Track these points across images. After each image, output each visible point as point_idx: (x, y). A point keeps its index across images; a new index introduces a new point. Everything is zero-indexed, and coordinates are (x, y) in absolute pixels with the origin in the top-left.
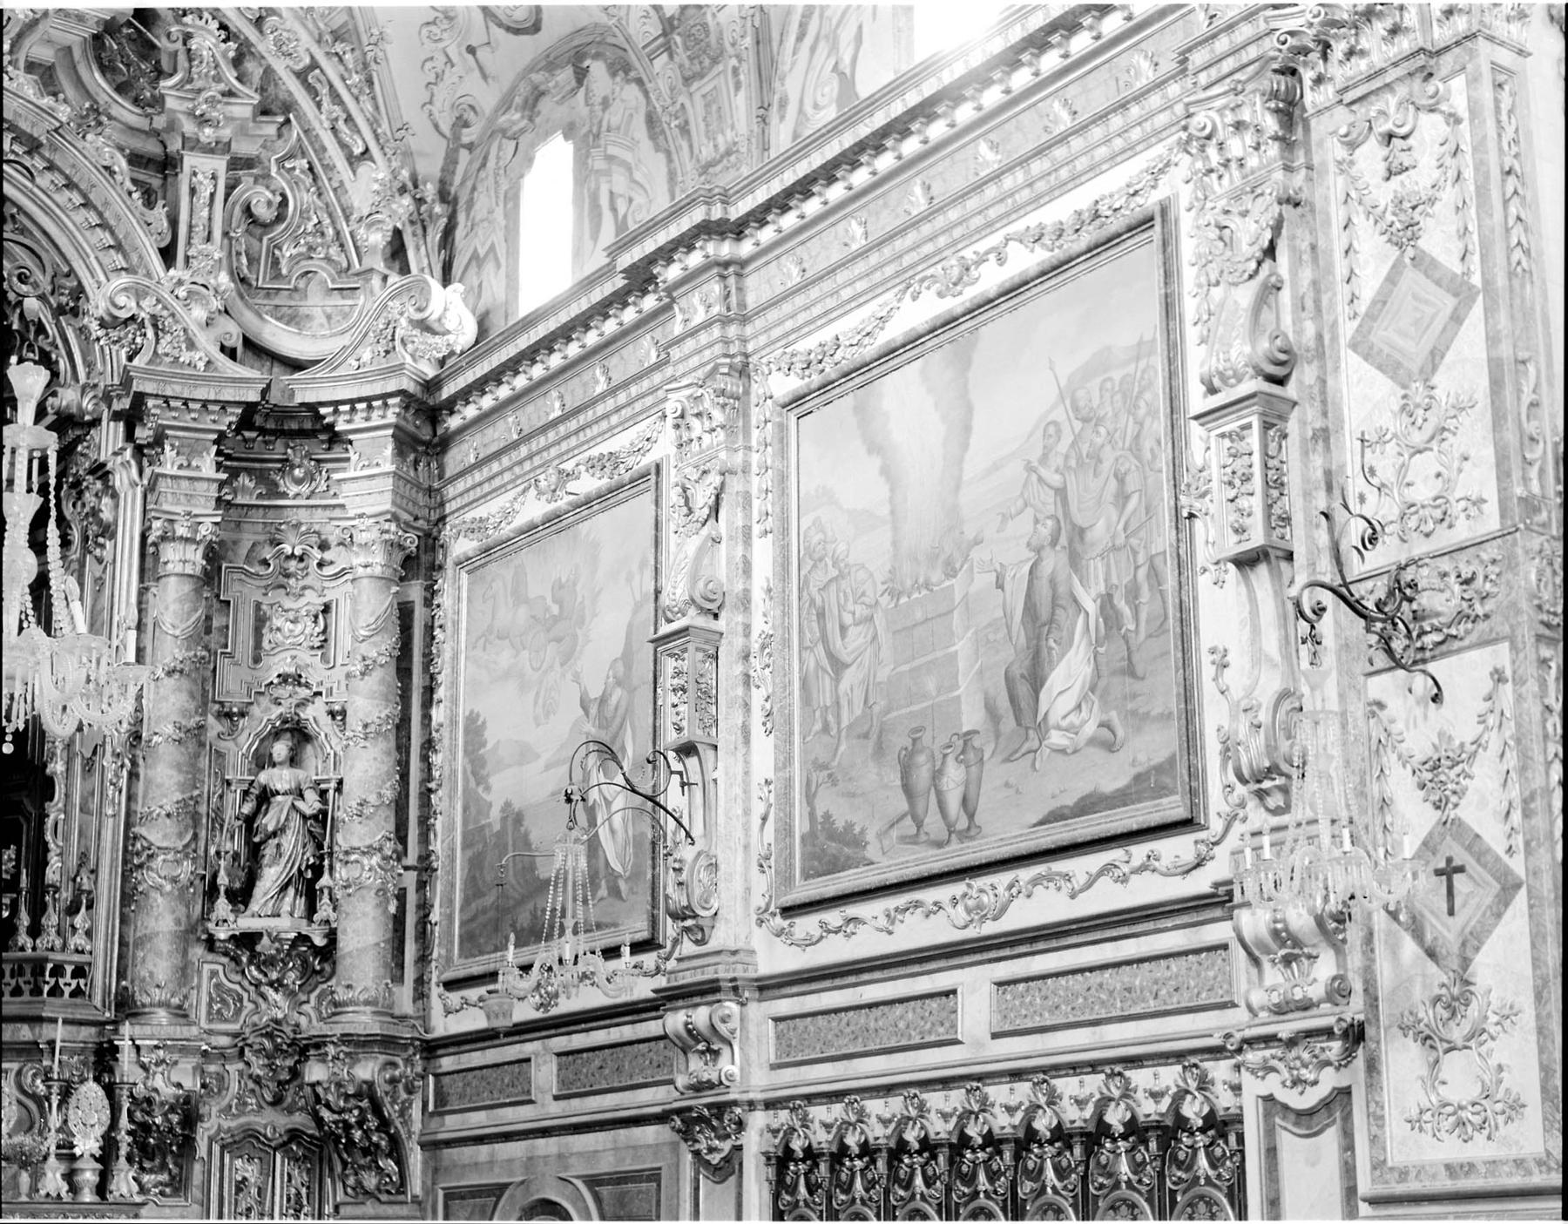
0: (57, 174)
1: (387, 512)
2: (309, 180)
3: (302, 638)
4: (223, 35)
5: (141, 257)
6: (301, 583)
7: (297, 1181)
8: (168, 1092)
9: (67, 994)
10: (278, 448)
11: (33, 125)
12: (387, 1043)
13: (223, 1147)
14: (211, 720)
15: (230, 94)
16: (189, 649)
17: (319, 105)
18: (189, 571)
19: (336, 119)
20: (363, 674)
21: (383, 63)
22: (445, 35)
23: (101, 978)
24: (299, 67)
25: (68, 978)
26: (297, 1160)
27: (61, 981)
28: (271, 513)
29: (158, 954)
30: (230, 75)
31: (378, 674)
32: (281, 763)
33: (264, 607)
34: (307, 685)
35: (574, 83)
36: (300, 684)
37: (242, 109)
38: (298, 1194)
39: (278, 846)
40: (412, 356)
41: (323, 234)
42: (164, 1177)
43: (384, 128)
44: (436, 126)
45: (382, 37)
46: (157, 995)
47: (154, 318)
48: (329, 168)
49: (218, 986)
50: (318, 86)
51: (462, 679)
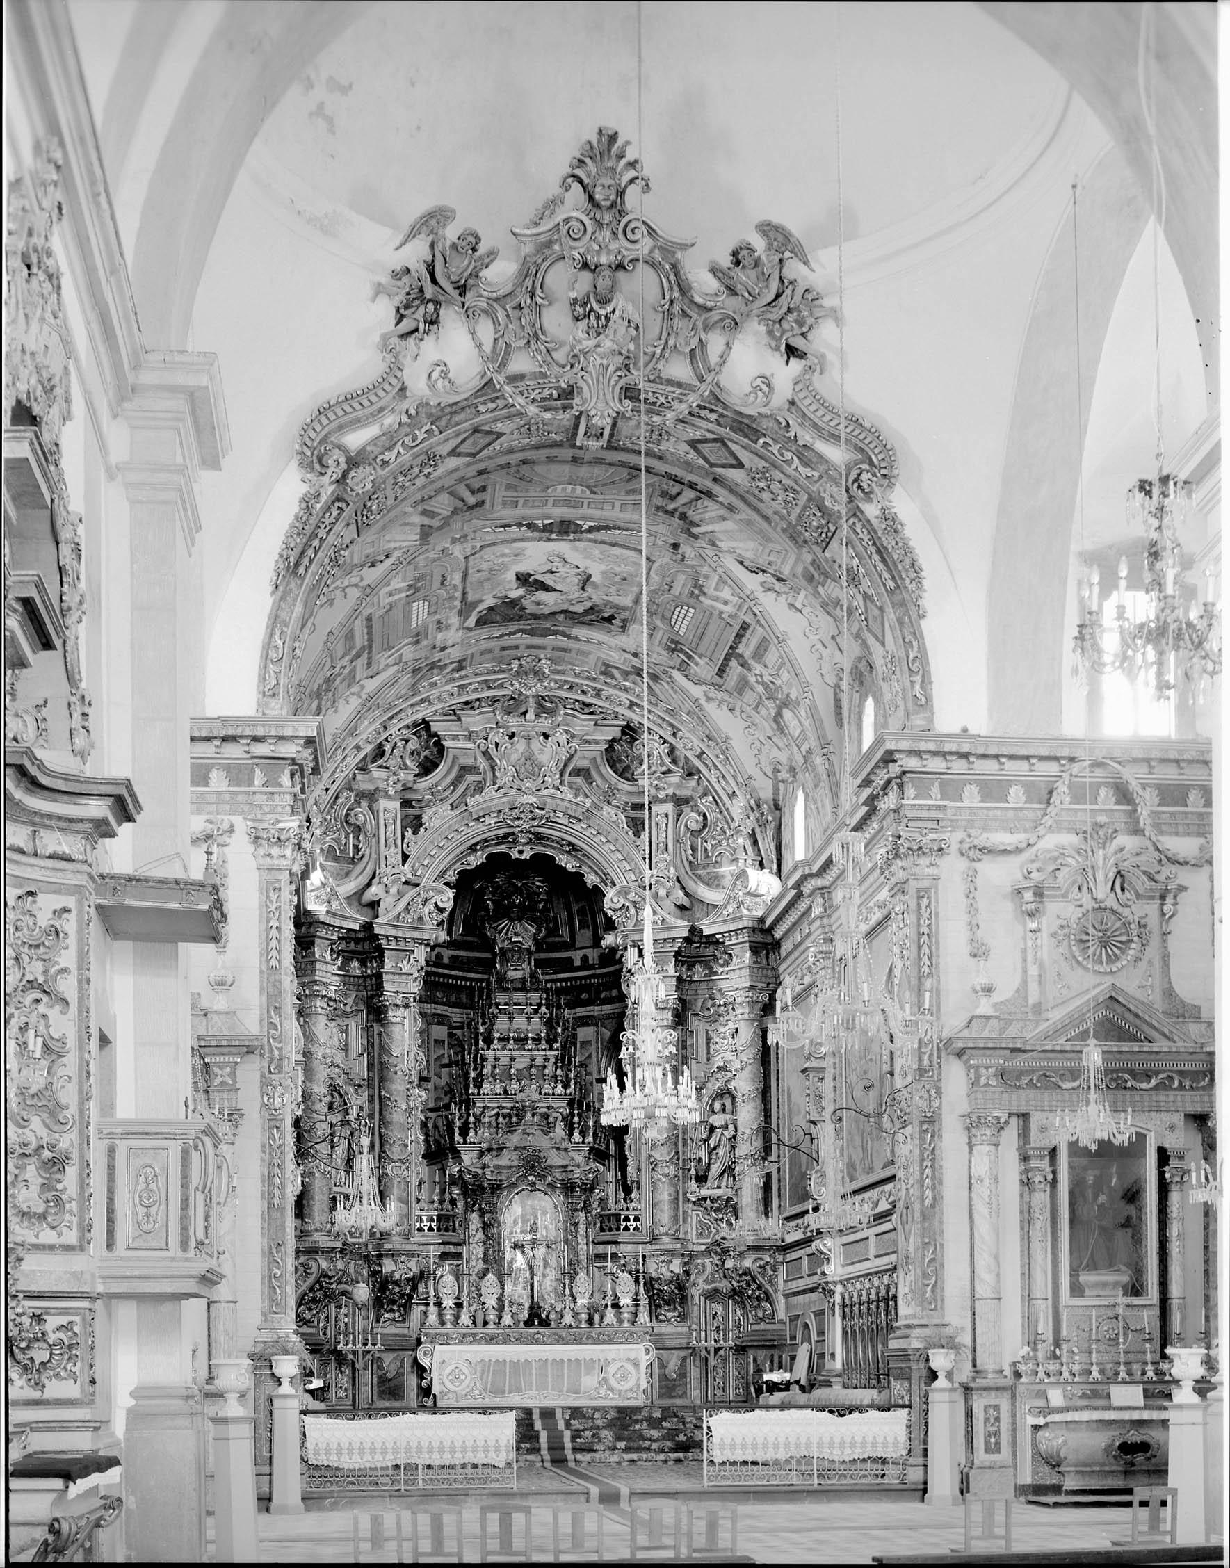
2: (714, 807)
8: (668, 1275)
12: (756, 1249)
15: (669, 771)
18: (665, 1023)
23: (645, 1222)
28: (711, 984)
29: (662, 1211)
30: (667, 760)
31: (748, 1069)
42: (676, 1314)
43: (740, 779)
45: (727, 738)
46: (663, 1230)
47: (634, 903)
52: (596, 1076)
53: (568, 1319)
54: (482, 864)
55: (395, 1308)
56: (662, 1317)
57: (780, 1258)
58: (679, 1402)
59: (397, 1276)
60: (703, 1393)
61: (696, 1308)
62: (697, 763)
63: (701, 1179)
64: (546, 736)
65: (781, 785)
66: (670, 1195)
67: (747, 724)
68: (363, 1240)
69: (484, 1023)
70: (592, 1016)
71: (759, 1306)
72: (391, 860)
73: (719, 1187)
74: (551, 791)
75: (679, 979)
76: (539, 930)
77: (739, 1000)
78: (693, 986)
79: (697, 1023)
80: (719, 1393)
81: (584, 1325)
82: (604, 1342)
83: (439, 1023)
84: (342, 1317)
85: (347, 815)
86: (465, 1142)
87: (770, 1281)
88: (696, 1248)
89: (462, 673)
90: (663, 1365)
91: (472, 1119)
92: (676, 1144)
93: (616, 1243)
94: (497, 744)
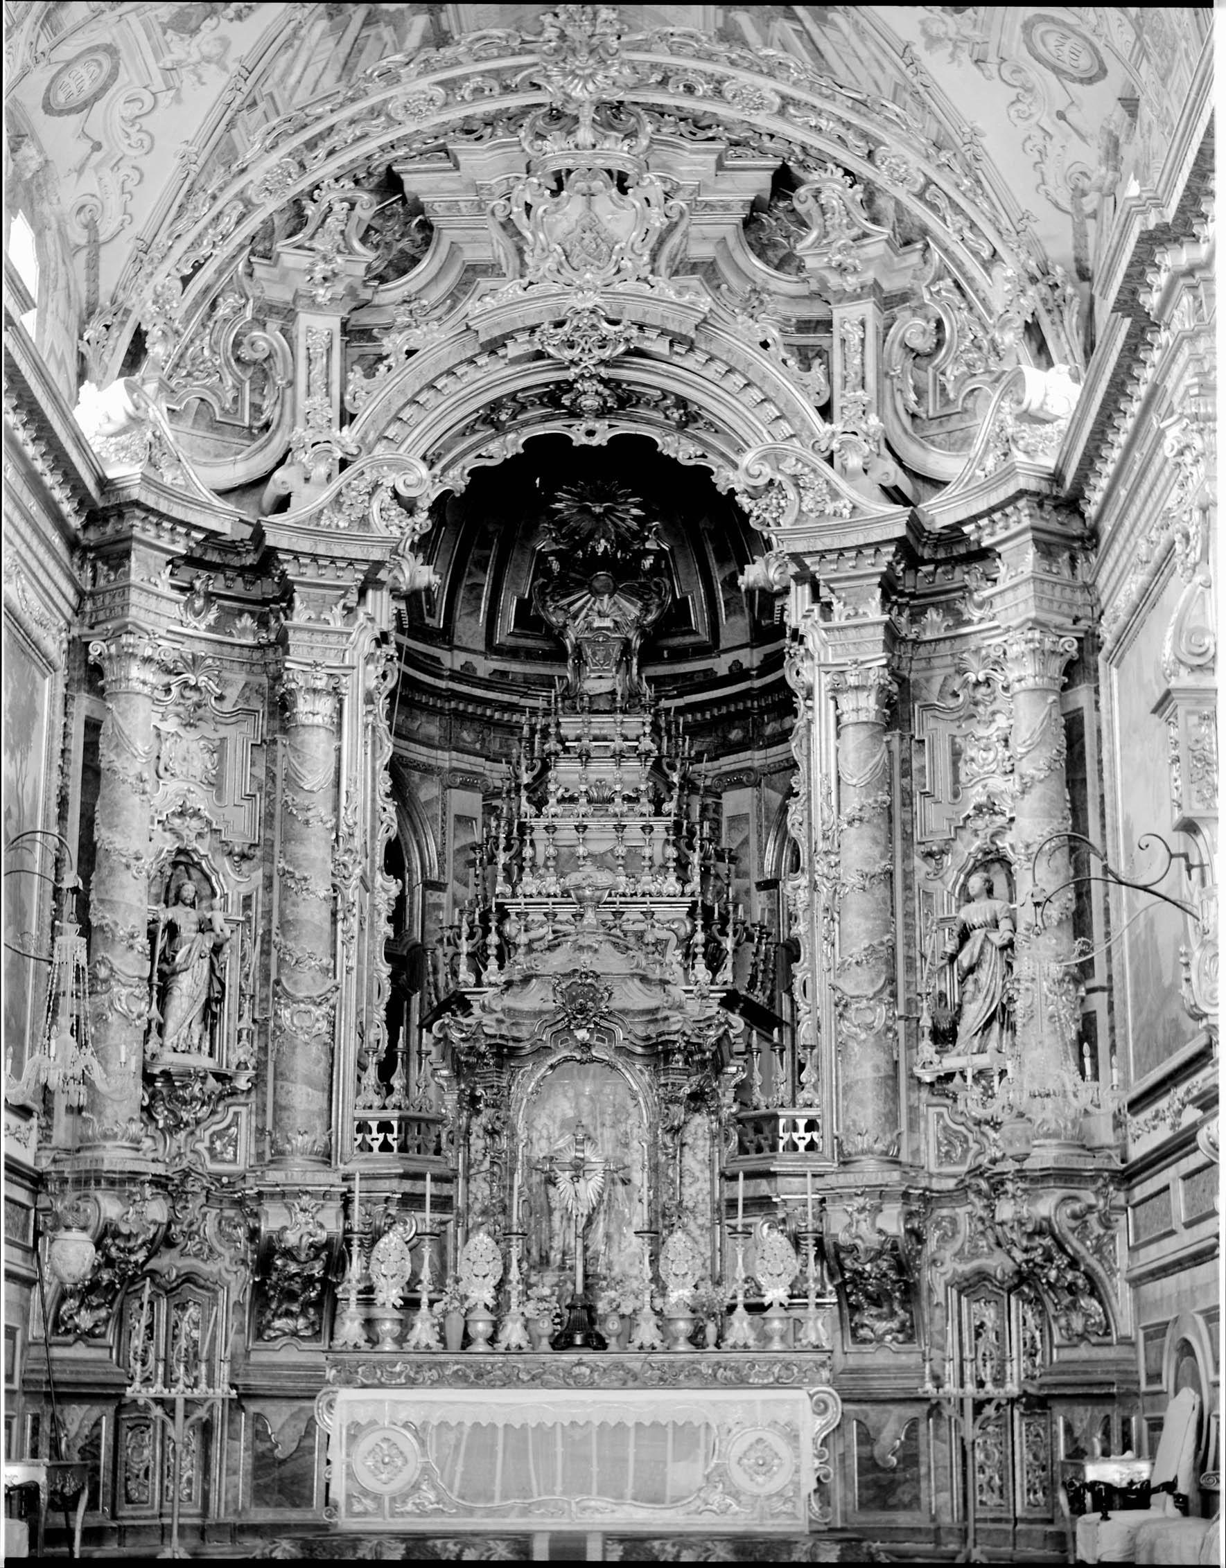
0: (719, 363)
1: (1028, 620)
2: (956, 298)
3: (993, 767)
4: (849, 180)
5: (803, 420)
6: (990, 709)
7: (1031, 1322)
8: (874, 1240)
9: (802, 1149)
10: (960, 575)
11: (681, 323)
12: (1065, 1176)
13: (960, 1292)
14: (917, 861)
15: (865, 235)
16: (868, 796)
17: (944, 220)
19: (961, 229)
20: (1023, 792)
21: (984, 158)
22: (1033, 109)
24: (917, 189)
25: (375, 1134)
26: (1030, 1302)
27: (368, 1138)
28: (958, 643)
29: (861, 1102)
30: (861, 215)
32: (977, 896)
33: (958, 740)
34: (1003, 814)
35: (1128, 119)
36: (995, 813)
37: (876, 248)
38: (1033, 1338)
39: (976, 981)
40: (1026, 452)
41: (980, 348)
42: (894, 1324)
43: (1005, 222)
44: (1056, 205)
46: (863, 1143)
48: (970, 280)
49: (946, 1128)
50: (937, 202)
51: (1119, 782)
52: (755, 878)
53: (647, 1332)
54: (517, 456)
55: (295, 1308)
56: (863, 1332)
57: (1120, 1198)
58: (903, 1519)
59: (291, 1239)
60: (958, 1500)
61: (938, 1313)
62: (919, 210)
63: (944, 1037)
64: (621, 182)
65: (1091, 225)
66: (877, 1068)
67: (1012, 94)
68: (240, 1167)
69: (530, 768)
70: (750, 769)
71: (1073, 1306)
72: (318, 420)
73: (981, 1051)
74: (631, 286)
75: (891, 630)
76: (646, 610)
77: (1013, 651)
78: (923, 651)
79: (931, 724)
80: (992, 1499)
81: (683, 1346)
82: (728, 1385)
83: (465, 786)
84: (185, 1327)
85: (237, 344)
86: (479, 983)
87: (1098, 1250)
88: (936, 1185)
89: (447, 52)
90: (866, 1438)
91: (493, 939)
92: (891, 962)
93: (770, 1175)
94: (528, 207)
